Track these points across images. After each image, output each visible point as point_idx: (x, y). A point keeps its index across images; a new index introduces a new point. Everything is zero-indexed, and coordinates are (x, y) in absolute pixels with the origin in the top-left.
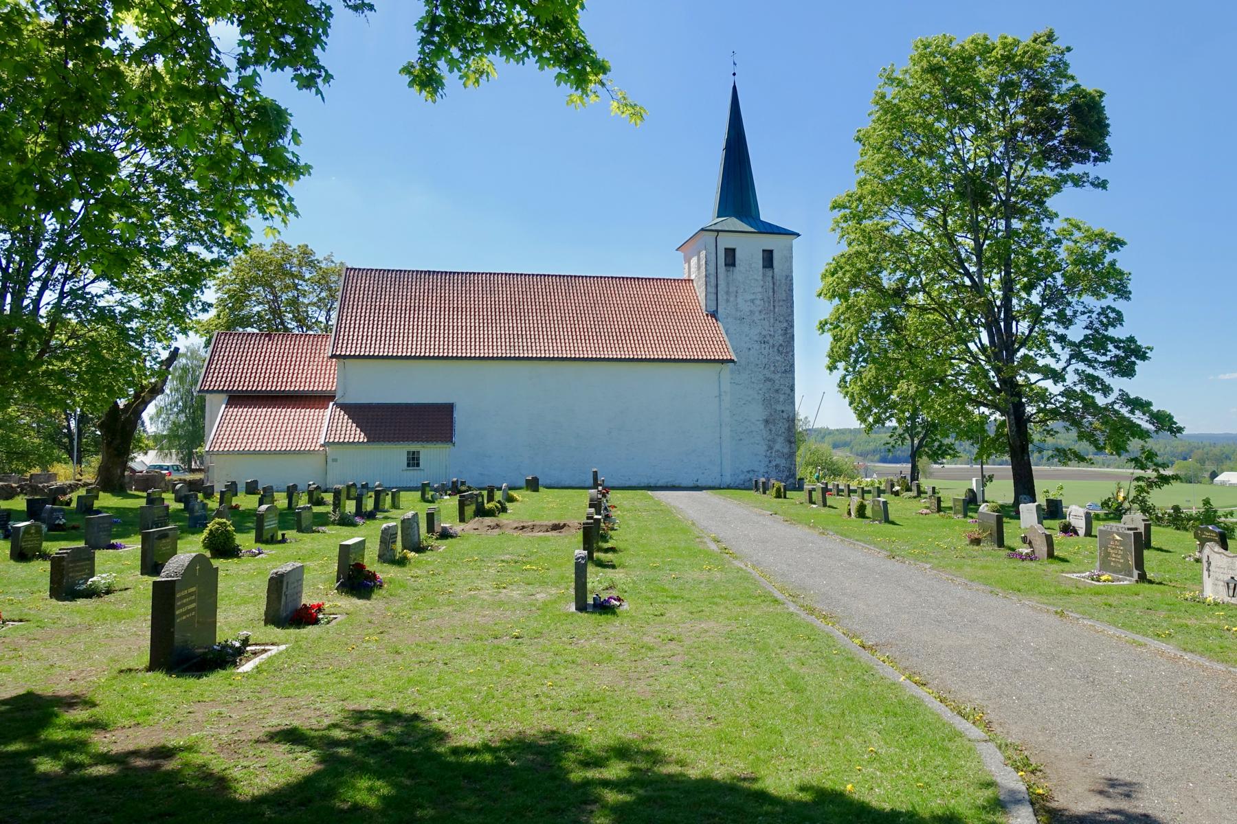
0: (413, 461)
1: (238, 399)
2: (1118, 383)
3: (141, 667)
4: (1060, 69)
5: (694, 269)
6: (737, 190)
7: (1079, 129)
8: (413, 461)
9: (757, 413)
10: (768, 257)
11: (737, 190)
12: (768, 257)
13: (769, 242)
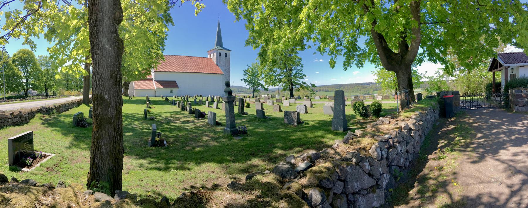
0: (171, 92)
2: (301, 80)
5: (213, 57)
6: (219, 43)
8: (171, 92)
11: (219, 43)
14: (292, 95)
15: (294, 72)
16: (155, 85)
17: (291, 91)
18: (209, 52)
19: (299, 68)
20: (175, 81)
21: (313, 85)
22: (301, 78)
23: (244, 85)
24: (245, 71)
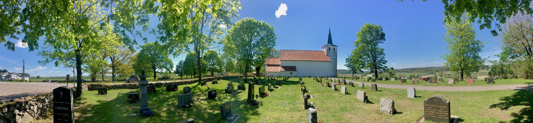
0: (291, 73)
1: (268, 65)
2: (384, 65)
3: (395, 107)
4: (381, 29)
5: (325, 50)
6: (330, 41)
7: (382, 36)
8: (291, 73)
9: (333, 68)
10: (334, 49)
11: (330, 41)
12: (334, 49)
13: (334, 47)
14: (377, 76)
15: (379, 59)
16: (280, 69)
17: (376, 72)
18: (323, 47)
19: (382, 56)
20: (295, 67)
21: (392, 69)
22: (384, 63)
23: (347, 68)
24: (347, 59)
